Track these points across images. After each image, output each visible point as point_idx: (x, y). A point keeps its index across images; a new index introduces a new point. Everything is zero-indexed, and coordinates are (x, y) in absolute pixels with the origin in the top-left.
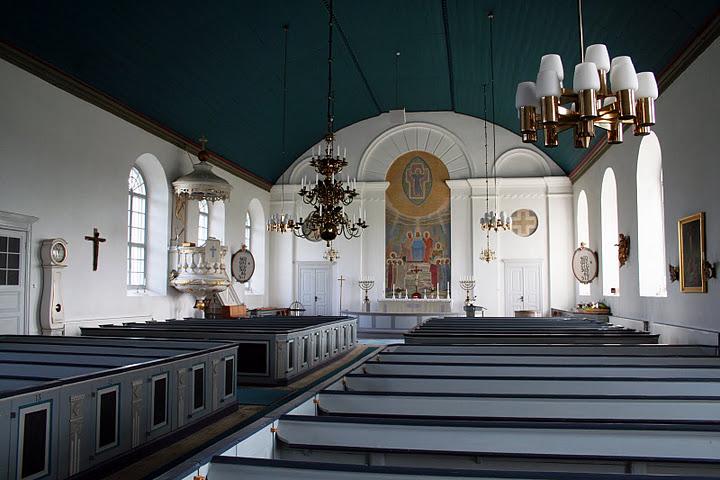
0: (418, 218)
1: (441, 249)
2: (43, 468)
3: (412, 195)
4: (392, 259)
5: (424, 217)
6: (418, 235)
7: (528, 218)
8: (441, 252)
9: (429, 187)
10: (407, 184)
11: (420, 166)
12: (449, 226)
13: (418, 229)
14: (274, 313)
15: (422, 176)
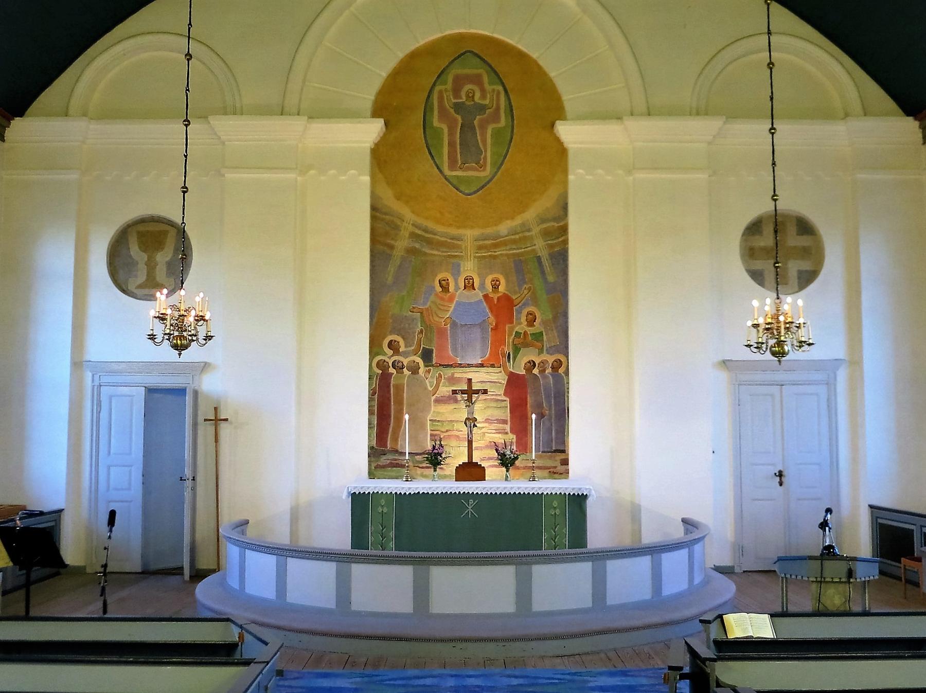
0: (469, 234)
1: (538, 327)
2: (454, 99)
3: (453, 165)
4: (388, 356)
5: (489, 231)
6: (469, 285)
7: (793, 240)
8: (538, 336)
9: (506, 140)
10: (438, 133)
11: (477, 80)
12: (561, 258)
13: (469, 268)
14: (55, 540)
15: (482, 108)
